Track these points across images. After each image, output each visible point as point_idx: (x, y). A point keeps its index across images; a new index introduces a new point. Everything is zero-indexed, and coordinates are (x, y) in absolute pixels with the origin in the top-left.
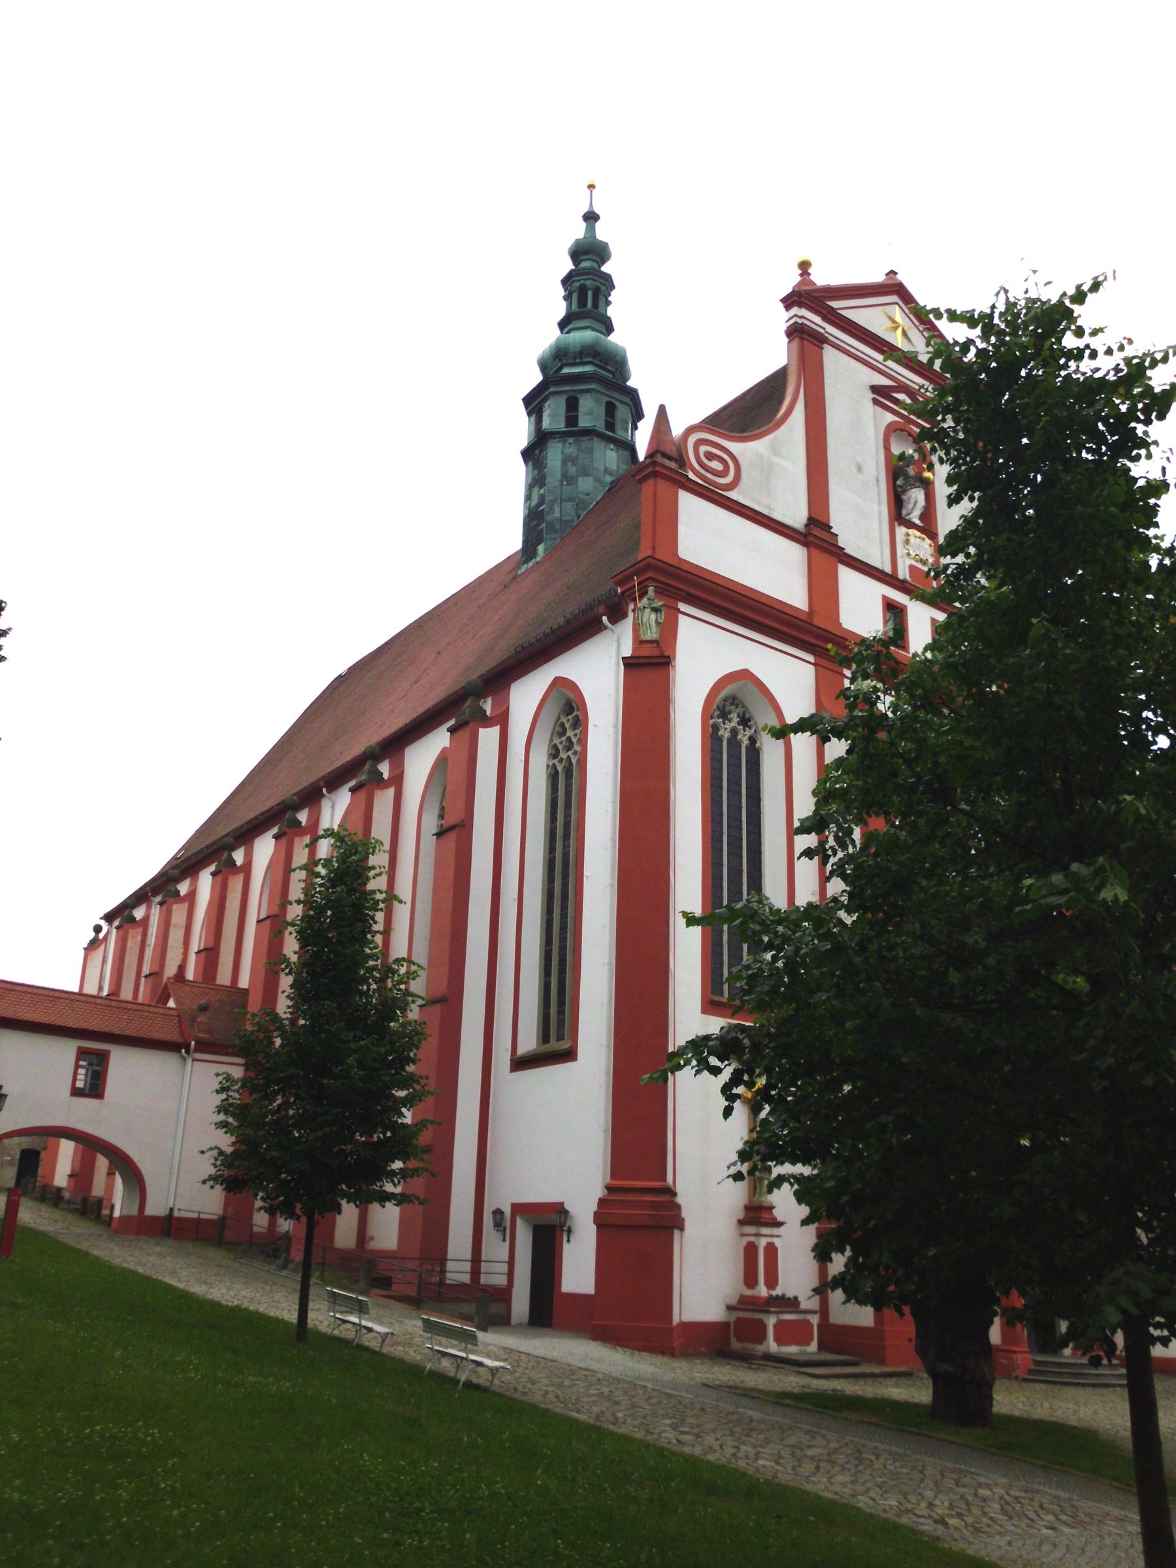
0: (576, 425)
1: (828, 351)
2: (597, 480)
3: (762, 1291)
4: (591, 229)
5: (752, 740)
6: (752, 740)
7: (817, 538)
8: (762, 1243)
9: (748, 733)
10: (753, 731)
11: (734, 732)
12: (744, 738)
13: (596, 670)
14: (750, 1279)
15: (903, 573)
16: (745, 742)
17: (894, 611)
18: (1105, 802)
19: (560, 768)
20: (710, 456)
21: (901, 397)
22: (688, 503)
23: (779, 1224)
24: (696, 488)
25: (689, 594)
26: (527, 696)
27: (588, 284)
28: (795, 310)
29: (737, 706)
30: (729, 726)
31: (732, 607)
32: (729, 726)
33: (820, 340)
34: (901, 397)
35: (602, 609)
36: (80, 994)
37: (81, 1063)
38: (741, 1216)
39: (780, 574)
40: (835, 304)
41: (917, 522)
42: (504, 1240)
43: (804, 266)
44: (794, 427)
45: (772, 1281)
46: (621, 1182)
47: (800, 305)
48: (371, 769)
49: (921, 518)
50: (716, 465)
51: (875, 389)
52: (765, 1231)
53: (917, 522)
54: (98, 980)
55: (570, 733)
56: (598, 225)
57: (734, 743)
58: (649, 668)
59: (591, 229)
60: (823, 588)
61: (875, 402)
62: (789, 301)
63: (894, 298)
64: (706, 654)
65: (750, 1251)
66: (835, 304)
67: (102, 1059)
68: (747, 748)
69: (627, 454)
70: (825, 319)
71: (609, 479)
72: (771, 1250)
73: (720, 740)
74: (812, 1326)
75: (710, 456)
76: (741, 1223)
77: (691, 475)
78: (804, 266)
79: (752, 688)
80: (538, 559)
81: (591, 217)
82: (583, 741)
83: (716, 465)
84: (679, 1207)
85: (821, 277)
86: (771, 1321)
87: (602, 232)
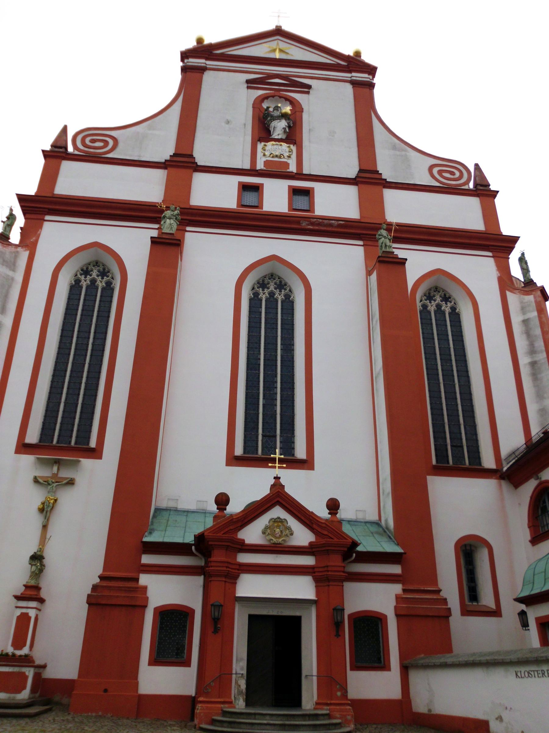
5: (287, 297)
6: (453, 309)
9: (449, 304)
10: (452, 303)
11: (439, 306)
12: (446, 308)
15: (260, 166)
20: (93, 141)
24: (151, 164)
25: (49, 209)
29: (439, 292)
31: (57, 207)
46: (109, 573)
57: (272, 298)
61: (248, 88)
68: (450, 314)
73: (444, 313)
74: (26, 677)
79: (444, 278)
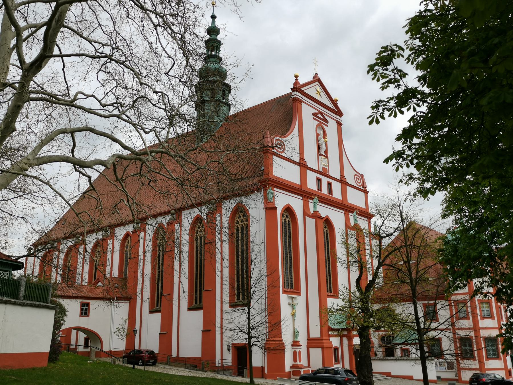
0: (488, 358)
1: (303, 103)
4: (213, 22)
7: (302, 165)
8: (298, 351)
11: (285, 220)
14: (295, 360)
15: (321, 170)
17: (319, 180)
18: (507, 258)
20: (279, 144)
21: (320, 116)
22: (275, 158)
23: (301, 346)
26: (229, 206)
27: (213, 43)
30: (284, 218)
32: (284, 218)
33: (301, 102)
34: (320, 116)
37: (74, 347)
38: (292, 343)
40: (303, 89)
41: (324, 154)
42: (296, 297)
43: (296, 77)
44: (296, 131)
48: (77, 236)
51: (314, 114)
52: (298, 347)
53: (324, 154)
55: (242, 218)
56: (216, 20)
58: (270, 209)
59: (213, 22)
60: (303, 177)
61: (314, 118)
63: (317, 83)
64: (282, 199)
66: (303, 89)
67: (87, 305)
70: (302, 94)
72: (300, 352)
76: (292, 346)
78: (296, 77)
81: (213, 17)
84: (284, 343)
87: (218, 23)
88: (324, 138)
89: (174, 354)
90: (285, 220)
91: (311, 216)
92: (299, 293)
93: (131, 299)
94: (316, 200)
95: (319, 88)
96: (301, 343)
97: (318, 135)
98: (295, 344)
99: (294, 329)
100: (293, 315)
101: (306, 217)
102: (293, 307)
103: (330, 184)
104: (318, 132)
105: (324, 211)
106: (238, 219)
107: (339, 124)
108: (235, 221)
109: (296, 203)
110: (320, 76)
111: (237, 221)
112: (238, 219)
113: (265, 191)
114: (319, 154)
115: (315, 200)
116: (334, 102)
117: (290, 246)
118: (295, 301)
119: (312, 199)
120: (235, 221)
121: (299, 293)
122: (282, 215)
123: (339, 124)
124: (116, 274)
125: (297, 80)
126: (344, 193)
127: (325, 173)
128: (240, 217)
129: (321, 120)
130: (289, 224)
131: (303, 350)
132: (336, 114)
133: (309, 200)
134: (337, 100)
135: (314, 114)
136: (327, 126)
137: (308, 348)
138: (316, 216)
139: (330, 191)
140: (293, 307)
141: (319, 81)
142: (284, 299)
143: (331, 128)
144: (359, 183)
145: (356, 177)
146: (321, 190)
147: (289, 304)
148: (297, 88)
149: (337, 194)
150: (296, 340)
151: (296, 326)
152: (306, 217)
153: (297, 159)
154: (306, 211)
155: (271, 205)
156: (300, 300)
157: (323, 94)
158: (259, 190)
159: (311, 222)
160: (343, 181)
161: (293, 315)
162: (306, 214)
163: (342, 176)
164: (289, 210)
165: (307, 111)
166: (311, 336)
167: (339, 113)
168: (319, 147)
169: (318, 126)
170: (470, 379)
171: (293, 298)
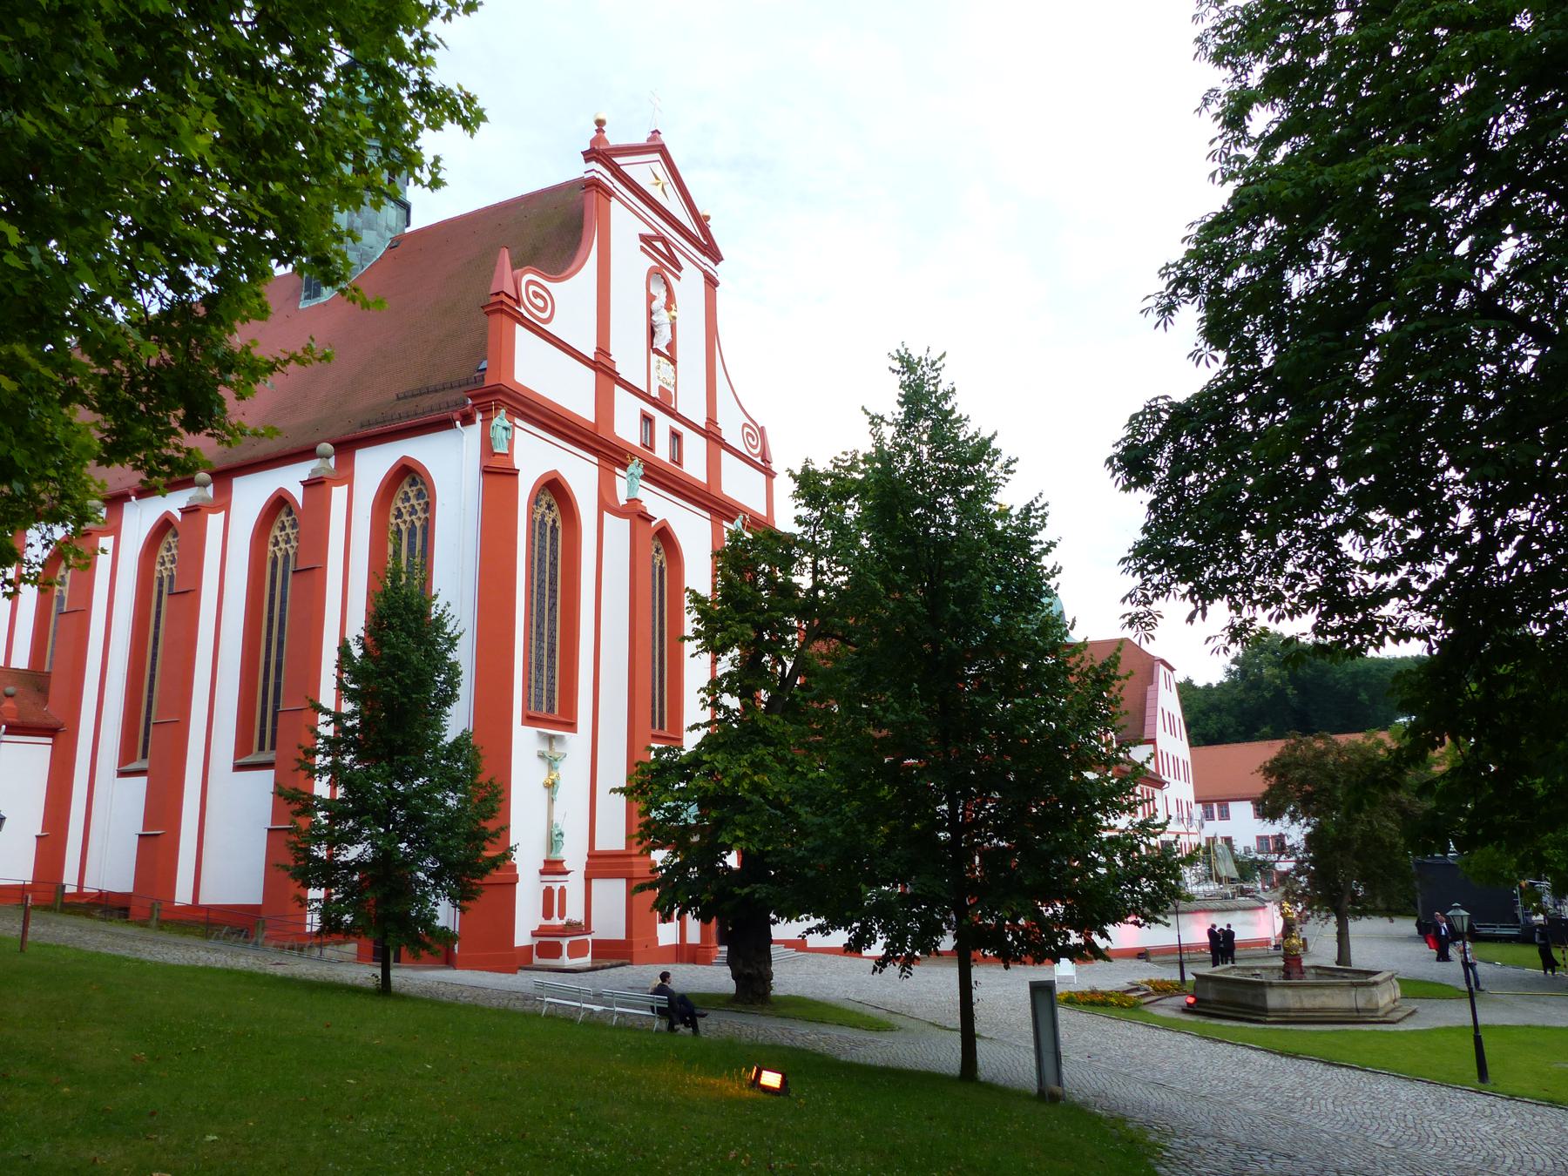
2: (381, 235)
3: (556, 921)
7: (603, 367)
8: (556, 887)
11: (543, 516)
13: (450, 459)
14: (547, 913)
15: (655, 393)
16: (550, 523)
17: (647, 419)
19: (403, 527)
20: (536, 295)
21: (659, 245)
22: (520, 330)
23: (567, 873)
26: (373, 465)
28: (594, 165)
33: (609, 193)
34: (659, 245)
35: (456, 415)
36: (771, 941)
39: (572, 391)
45: (562, 915)
47: (597, 161)
49: (668, 347)
50: (540, 303)
51: (644, 238)
54: (830, 957)
57: (543, 523)
58: (498, 472)
60: (604, 404)
61: (642, 249)
62: (589, 155)
63: (657, 156)
64: (535, 455)
65: (548, 893)
69: (404, 212)
70: (613, 174)
71: (389, 235)
72: (562, 891)
75: (536, 295)
76: (542, 873)
77: (522, 310)
80: (323, 300)
82: (429, 507)
83: (540, 303)
84: (514, 867)
85: (614, 138)
86: (565, 942)
88: (668, 308)
89: (183, 896)
90: (543, 516)
91: (619, 512)
92: (571, 726)
93: (57, 731)
94: (636, 468)
95: (660, 169)
96: (567, 866)
97: (651, 298)
98: (553, 867)
99: (550, 823)
100: (551, 786)
101: (606, 515)
102: (551, 762)
103: (676, 436)
104: (653, 291)
105: (660, 505)
106: (400, 505)
107: (711, 282)
108: (393, 511)
109: (581, 473)
110: (665, 138)
111: (399, 510)
112: (400, 505)
113: (487, 421)
114: (652, 348)
115: (631, 468)
116: (701, 221)
117: (553, 591)
118: (558, 749)
119: (624, 466)
120: (393, 511)
121: (571, 726)
122: (535, 500)
123: (711, 282)
124: (21, 660)
125: (600, 131)
126: (713, 466)
127: (664, 404)
128: (408, 499)
129: (665, 264)
130: (554, 529)
131: (574, 885)
132: (704, 254)
133: (618, 470)
134: (707, 218)
135: (644, 238)
136: (678, 278)
137: (588, 880)
138: (637, 514)
139: (677, 459)
140: (551, 762)
141: (662, 150)
142: (525, 740)
143: (689, 284)
144: (755, 447)
145: (747, 430)
146: (652, 449)
147: (542, 756)
148: (598, 153)
149: (694, 466)
150: (554, 857)
151: (557, 818)
152: (606, 515)
153: (590, 351)
154: (607, 498)
155: (496, 463)
156: (576, 744)
157: (671, 190)
158: (467, 420)
159: (618, 530)
160: (712, 435)
161: (551, 786)
162: (606, 504)
163: (711, 420)
164: (554, 488)
165: (625, 225)
166: (598, 848)
167: (716, 257)
168: (652, 333)
169: (652, 273)
170: (101, 894)
171: (551, 738)
